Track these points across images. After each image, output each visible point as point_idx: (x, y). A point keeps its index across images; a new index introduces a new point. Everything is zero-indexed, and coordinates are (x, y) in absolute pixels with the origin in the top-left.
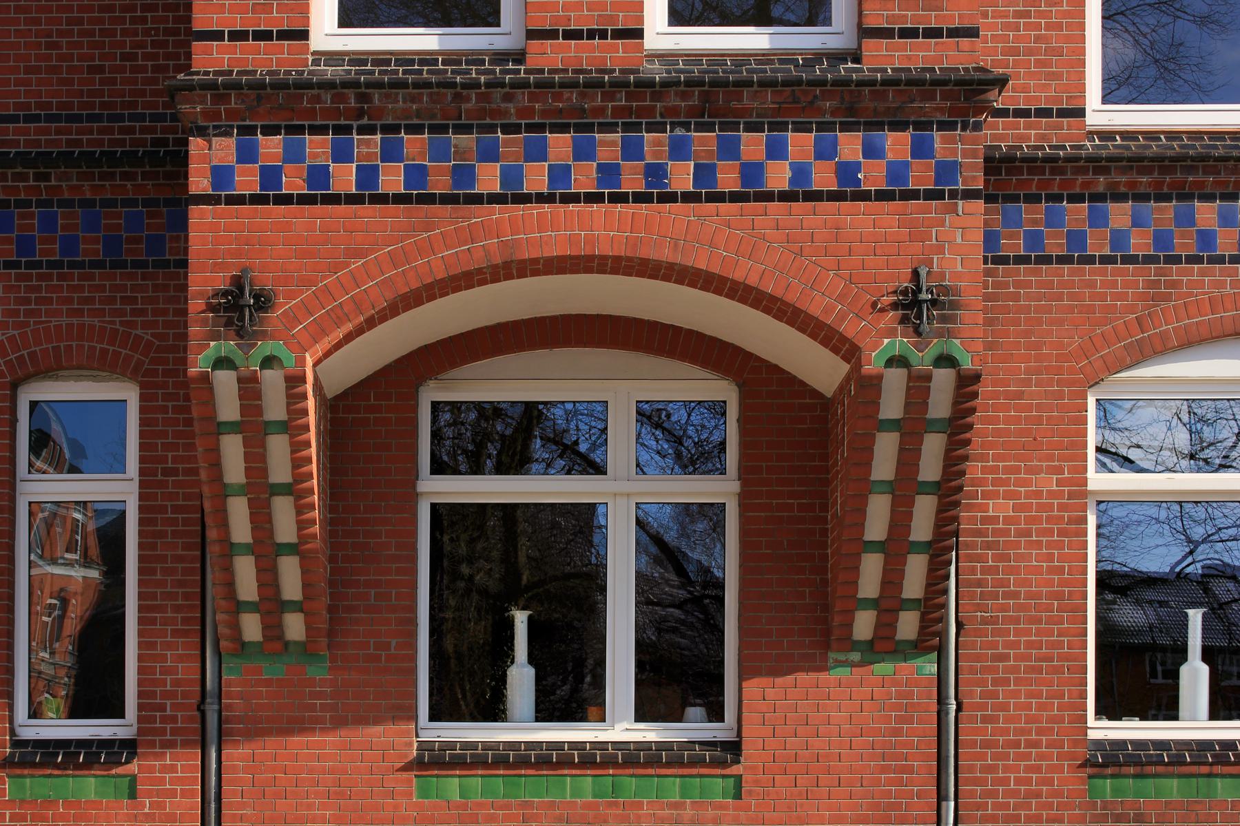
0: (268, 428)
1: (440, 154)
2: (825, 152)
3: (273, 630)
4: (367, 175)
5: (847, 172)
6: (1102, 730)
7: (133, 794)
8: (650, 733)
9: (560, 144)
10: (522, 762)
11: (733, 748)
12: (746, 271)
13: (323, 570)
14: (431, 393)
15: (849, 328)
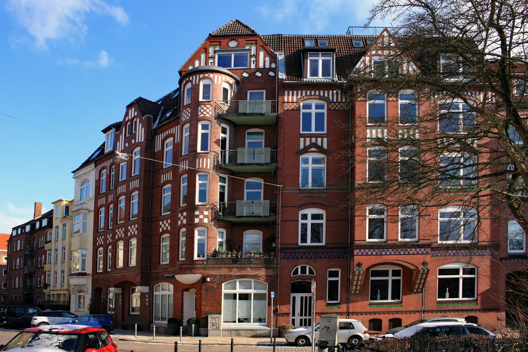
1: (379, 251)
2: (416, 250)
3: (355, 292)
4: (372, 253)
5: (418, 252)
6: (438, 299)
7: (340, 308)
8: (392, 301)
9: (390, 250)
10: (378, 304)
11: (401, 302)
12: (408, 261)
13: (361, 287)
14: (371, 269)
15: (418, 266)
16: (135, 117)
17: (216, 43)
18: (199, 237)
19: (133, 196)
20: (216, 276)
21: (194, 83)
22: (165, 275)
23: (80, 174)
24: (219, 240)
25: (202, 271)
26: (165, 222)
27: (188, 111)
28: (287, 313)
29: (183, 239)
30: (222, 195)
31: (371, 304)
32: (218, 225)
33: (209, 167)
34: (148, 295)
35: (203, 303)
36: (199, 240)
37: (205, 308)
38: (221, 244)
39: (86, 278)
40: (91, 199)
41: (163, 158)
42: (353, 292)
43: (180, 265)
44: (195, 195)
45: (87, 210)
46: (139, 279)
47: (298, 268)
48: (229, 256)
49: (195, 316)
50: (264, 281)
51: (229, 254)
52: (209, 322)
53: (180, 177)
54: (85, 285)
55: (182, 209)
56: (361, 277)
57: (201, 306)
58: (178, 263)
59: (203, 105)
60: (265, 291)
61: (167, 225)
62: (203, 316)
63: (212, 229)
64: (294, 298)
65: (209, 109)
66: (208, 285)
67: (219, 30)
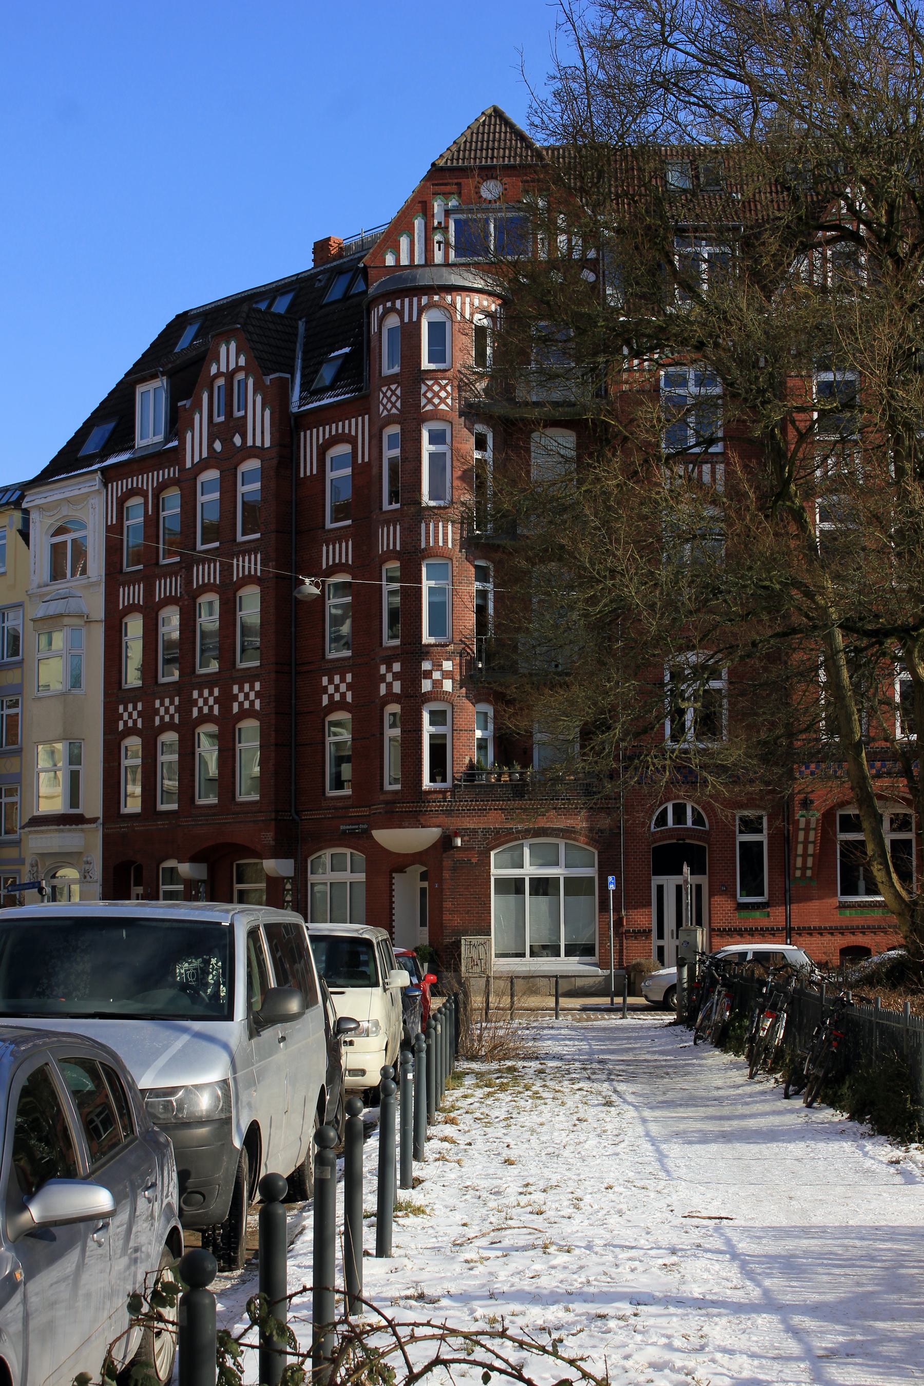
0: (811, 829)
3: (803, 874)
7: (769, 916)
14: (839, 812)
16: (238, 369)
17: (447, 189)
18: (433, 729)
19: (128, 508)
20: (475, 831)
21: (406, 320)
22: (342, 827)
23: (49, 499)
24: (479, 734)
25: (442, 819)
26: (337, 679)
27: (393, 393)
28: (644, 931)
29: (392, 733)
30: (481, 610)
31: (843, 906)
32: (475, 696)
33: (450, 546)
34: (292, 884)
35: (447, 905)
36: (432, 736)
37: (452, 920)
38: (484, 744)
39: (82, 830)
40: (96, 584)
41: (381, 576)
42: (798, 873)
43: (387, 803)
44: (421, 625)
45: (81, 616)
46: (269, 837)
47: (666, 809)
48: (505, 778)
49: (427, 943)
50: (586, 844)
51: (504, 773)
52: (463, 956)
53: (381, 567)
54: (81, 853)
55: (390, 653)
56: (812, 834)
57: (441, 912)
58: (382, 798)
59: (431, 379)
60: (590, 872)
61: (343, 688)
62: (447, 940)
63: (462, 709)
64: (660, 888)
65: (447, 392)
66: (458, 855)
67: (454, 149)
